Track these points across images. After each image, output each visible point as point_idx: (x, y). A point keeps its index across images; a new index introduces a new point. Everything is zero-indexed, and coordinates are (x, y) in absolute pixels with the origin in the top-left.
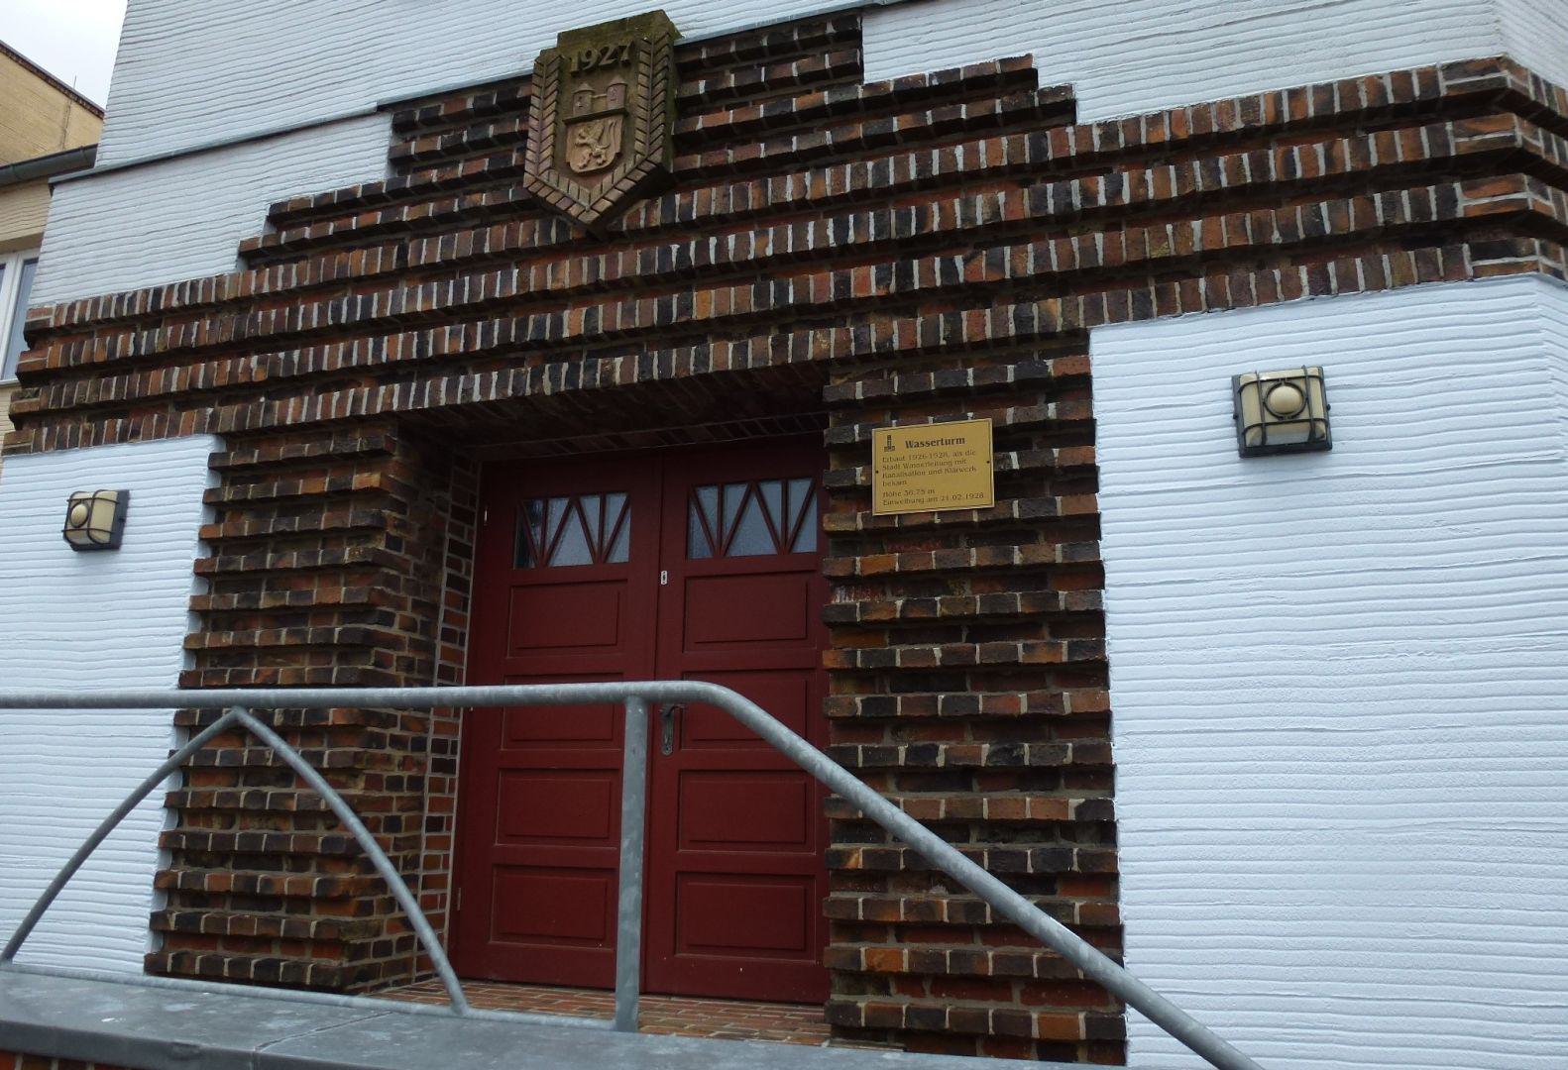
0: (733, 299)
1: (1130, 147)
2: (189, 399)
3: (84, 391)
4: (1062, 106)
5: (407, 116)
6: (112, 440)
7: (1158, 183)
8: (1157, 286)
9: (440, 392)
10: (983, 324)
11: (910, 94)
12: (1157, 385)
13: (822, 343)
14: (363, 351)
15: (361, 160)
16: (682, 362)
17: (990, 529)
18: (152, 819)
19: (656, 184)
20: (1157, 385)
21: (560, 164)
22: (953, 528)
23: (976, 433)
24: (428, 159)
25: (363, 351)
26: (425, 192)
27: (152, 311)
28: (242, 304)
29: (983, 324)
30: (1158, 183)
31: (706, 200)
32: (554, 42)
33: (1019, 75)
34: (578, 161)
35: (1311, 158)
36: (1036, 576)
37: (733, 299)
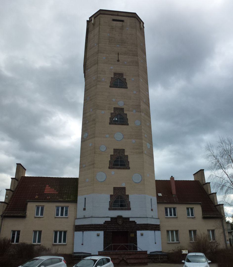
0: (125, 228)
1: (138, 225)
2: (102, 229)
3: (90, 228)
4: (136, 223)
5: (111, 218)
6: (98, 231)
7: (139, 226)
8: (139, 230)
9: (114, 230)
10: (134, 230)
11: (131, 221)
12: (139, 233)
13: (129, 230)
14: (110, 228)
15: (109, 220)
16: (124, 230)
17: (134, 237)
18: (141, 250)
19: (122, 224)
20: (139, 233)
21: (119, 222)
22: (133, 237)
23: (134, 234)
24: (112, 220)
25: (110, 228)
26: (112, 222)
27: (99, 225)
28: (104, 225)
29: (134, 230)
30: (139, 226)
31: (124, 224)
32: (136, 222)
33: (135, 221)
34: (120, 222)
35: (143, 226)
36: (135, 239)
37: (125, 228)
